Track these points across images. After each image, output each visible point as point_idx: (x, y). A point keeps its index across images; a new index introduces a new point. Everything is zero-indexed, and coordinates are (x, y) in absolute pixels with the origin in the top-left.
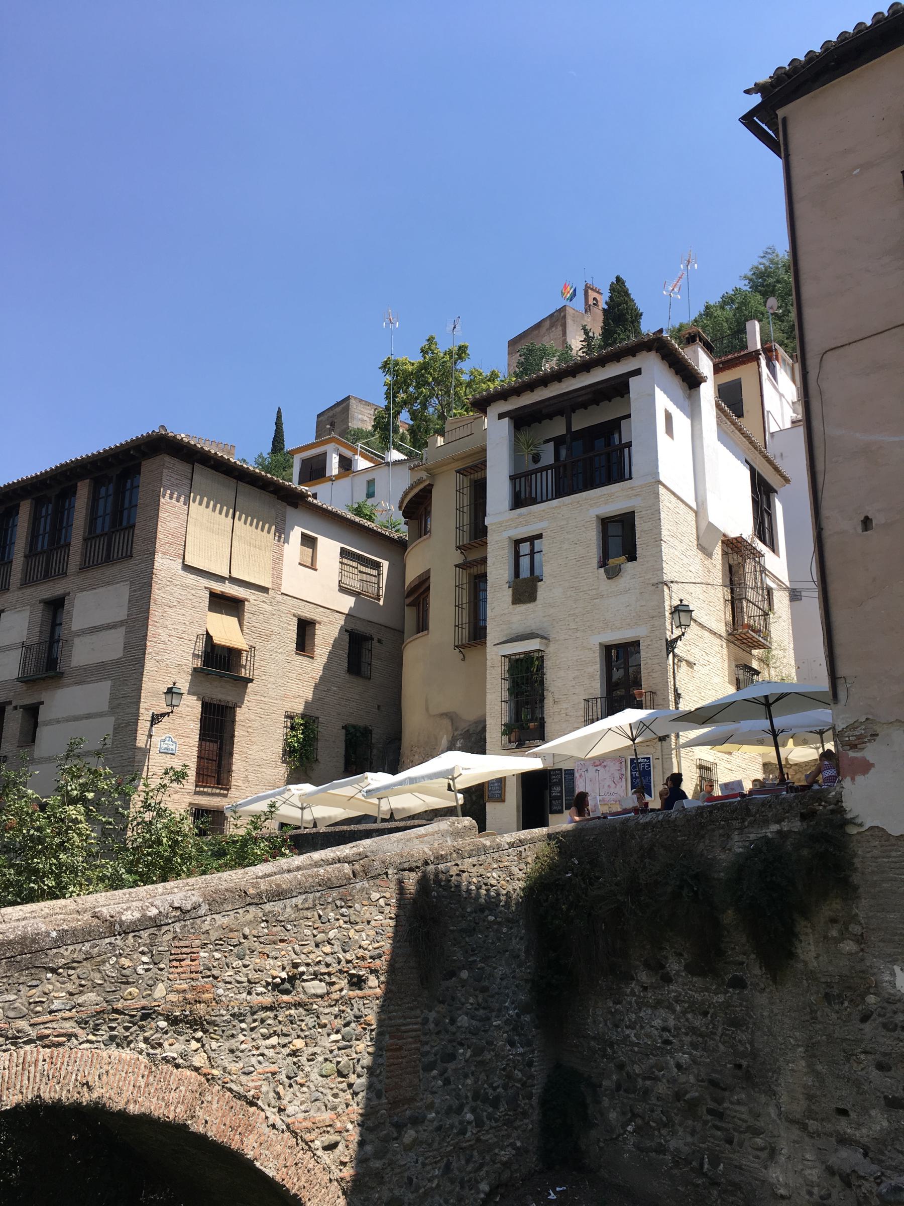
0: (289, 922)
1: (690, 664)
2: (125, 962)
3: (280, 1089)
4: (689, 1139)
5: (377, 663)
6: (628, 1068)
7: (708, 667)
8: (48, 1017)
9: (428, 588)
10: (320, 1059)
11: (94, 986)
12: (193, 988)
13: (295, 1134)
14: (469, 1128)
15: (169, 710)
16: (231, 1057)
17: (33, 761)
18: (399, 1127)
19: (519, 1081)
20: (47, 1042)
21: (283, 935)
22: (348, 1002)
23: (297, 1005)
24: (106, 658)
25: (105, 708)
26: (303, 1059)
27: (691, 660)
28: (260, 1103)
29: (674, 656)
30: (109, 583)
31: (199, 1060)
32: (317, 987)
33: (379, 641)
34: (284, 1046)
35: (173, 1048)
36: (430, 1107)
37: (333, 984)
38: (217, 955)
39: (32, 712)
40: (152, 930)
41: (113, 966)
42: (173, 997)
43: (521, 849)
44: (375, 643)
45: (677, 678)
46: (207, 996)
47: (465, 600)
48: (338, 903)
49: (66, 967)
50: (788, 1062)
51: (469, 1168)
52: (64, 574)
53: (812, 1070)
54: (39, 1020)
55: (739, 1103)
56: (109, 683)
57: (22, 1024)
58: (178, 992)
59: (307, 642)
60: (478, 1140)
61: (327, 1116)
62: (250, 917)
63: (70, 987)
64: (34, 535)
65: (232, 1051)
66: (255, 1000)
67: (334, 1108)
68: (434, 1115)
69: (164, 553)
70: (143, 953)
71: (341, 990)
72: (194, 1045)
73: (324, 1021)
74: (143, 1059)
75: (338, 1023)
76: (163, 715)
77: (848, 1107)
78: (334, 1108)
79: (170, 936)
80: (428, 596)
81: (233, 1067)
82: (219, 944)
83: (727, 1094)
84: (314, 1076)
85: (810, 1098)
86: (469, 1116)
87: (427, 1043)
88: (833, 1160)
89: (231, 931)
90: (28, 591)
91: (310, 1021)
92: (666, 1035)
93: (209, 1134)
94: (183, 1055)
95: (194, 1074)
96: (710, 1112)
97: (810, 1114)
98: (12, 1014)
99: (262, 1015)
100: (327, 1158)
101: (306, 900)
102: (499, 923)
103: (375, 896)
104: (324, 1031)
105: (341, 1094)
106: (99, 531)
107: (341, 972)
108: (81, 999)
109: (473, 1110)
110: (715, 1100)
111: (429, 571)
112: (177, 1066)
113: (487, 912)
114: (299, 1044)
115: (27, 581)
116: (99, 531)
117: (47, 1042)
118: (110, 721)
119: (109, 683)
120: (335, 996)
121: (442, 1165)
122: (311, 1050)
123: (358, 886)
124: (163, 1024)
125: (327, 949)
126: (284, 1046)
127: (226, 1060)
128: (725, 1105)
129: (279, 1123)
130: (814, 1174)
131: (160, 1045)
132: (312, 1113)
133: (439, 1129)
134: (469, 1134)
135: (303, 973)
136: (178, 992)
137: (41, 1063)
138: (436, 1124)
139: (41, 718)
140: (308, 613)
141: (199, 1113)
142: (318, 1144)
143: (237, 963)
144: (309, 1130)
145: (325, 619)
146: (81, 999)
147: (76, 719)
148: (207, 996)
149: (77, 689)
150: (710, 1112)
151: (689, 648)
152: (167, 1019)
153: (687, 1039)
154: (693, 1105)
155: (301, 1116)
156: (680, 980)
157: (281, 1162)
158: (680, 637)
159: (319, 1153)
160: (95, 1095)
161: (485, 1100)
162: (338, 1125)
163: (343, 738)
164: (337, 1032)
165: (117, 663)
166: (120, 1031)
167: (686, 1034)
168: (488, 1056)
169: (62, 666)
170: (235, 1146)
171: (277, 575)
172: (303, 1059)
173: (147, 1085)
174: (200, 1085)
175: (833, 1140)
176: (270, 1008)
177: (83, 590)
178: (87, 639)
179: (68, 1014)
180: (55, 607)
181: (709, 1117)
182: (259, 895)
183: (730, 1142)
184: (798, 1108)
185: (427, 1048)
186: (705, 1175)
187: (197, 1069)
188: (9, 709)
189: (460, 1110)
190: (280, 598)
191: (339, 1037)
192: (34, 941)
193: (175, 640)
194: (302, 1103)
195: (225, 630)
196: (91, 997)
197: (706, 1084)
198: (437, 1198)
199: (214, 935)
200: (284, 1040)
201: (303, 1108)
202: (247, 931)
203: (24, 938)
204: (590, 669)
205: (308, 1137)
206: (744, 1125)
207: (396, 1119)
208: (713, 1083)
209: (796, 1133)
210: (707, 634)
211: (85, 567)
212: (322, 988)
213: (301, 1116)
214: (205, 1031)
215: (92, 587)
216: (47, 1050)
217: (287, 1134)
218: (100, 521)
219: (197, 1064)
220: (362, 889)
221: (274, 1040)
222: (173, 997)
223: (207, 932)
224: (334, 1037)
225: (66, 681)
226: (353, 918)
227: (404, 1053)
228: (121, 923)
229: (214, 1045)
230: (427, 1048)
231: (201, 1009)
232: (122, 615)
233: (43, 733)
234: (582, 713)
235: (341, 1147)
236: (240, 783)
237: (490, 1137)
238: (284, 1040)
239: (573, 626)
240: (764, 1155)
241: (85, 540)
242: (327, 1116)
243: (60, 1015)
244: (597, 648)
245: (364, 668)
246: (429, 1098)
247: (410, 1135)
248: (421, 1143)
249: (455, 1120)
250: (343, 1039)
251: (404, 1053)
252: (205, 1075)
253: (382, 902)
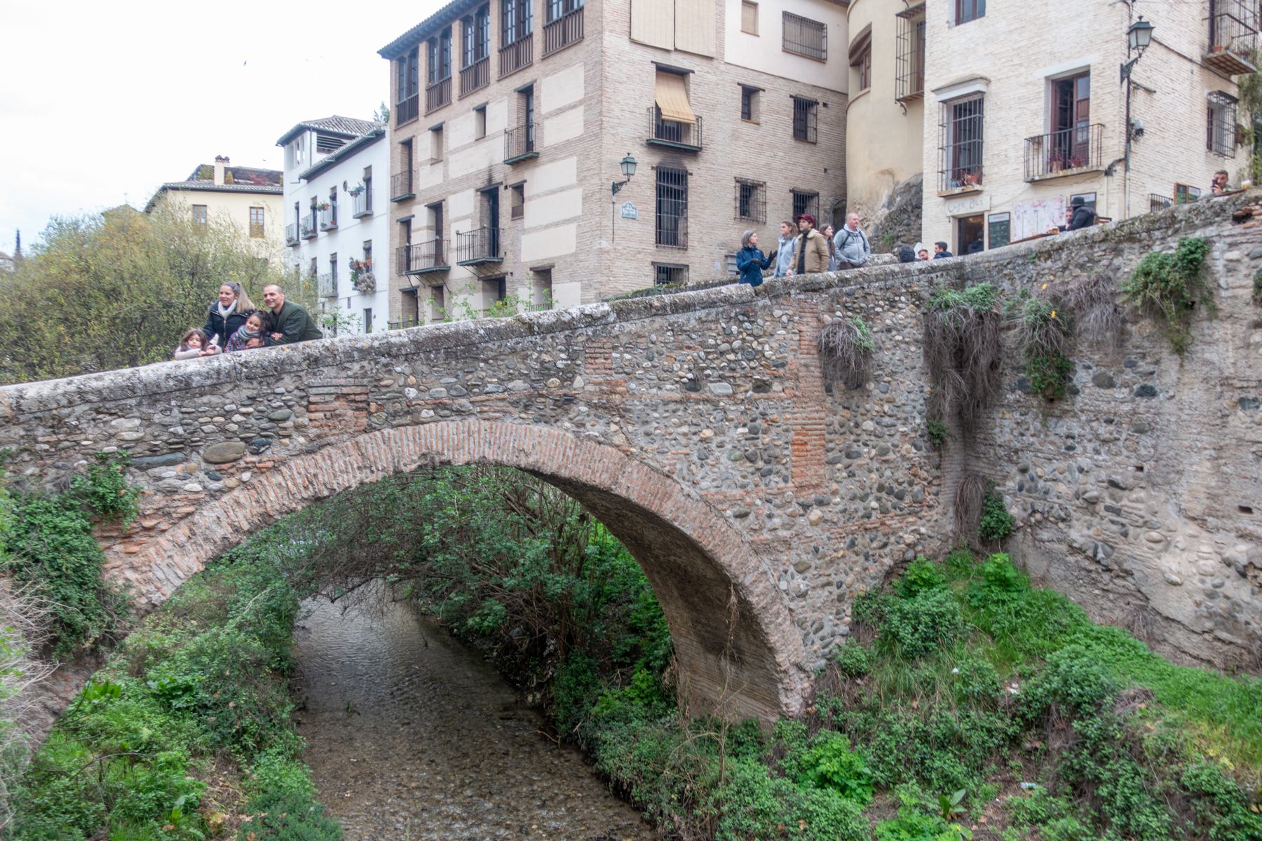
0: (694, 332)
1: (1149, 91)
2: (546, 358)
3: (693, 467)
4: (1085, 532)
5: (821, 122)
6: (1031, 472)
7: (1173, 96)
8: (483, 397)
9: (869, 45)
10: (729, 446)
11: (521, 374)
12: (608, 383)
13: (707, 503)
14: (874, 513)
15: (625, 178)
16: (648, 439)
17: (524, 231)
18: (806, 507)
19: (925, 479)
20: (485, 415)
21: (688, 343)
22: (752, 401)
23: (706, 401)
24: (570, 137)
25: (574, 180)
26: (713, 446)
27: (1152, 87)
28: (675, 477)
29: (1129, 83)
30: (567, 66)
31: (619, 439)
32: (723, 388)
33: (825, 105)
34: (695, 434)
35: (595, 429)
36: (835, 493)
37: (739, 386)
38: (627, 356)
39: (519, 188)
40: (567, 332)
41: (536, 360)
42: (590, 388)
43: (933, 275)
44: (820, 107)
45: (1131, 107)
46: (620, 389)
47: (907, 49)
48: (741, 318)
49: (495, 358)
50: (1191, 465)
51: (874, 545)
52: (531, 65)
53: (1217, 470)
54: (479, 398)
55: (1137, 501)
56: (575, 158)
57: (464, 401)
58: (595, 384)
59: (753, 109)
60: (883, 524)
61: (737, 492)
62: (656, 325)
63: (502, 375)
64: (431, 65)
65: (647, 434)
66: (664, 394)
67: (743, 487)
68: (838, 500)
69: (611, 31)
70: (561, 351)
71: (746, 391)
72: (613, 427)
73: (731, 416)
74: (570, 435)
75: (745, 419)
76: (621, 184)
77: (1253, 505)
78: (743, 487)
79: (584, 338)
80: (869, 55)
81: (649, 447)
82: (629, 348)
83: (1126, 493)
84: (724, 459)
85: (1212, 497)
86: (874, 504)
87: (831, 441)
88: (1229, 553)
89: (639, 336)
90: (505, 82)
91: (720, 415)
92: (1070, 442)
93: (632, 497)
94: (604, 435)
95: (614, 450)
96: (1108, 509)
97: (1212, 512)
98: (453, 393)
99: (672, 406)
100: (737, 524)
101: (708, 314)
102: (907, 343)
103: (777, 313)
104: (732, 424)
105: (750, 476)
106: (555, 17)
107: (746, 376)
108: (510, 385)
109: (878, 499)
110: (1112, 497)
111: (870, 26)
112: (600, 443)
113: (894, 333)
114: (708, 433)
115: (504, 75)
116: (555, 17)
117: (485, 415)
118: (578, 193)
119: (575, 158)
120: (740, 396)
121: (848, 541)
122: (719, 439)
123: (760, 304)
124: (584, 409)
125: (731, 357)
126: (695, 434)
127: (642, 440)
128: (1123, 503)
129: (693, 494)
130: (1211, 564)
131: (584, 425)
132: (723, 489)
133: (844, 511)
134: (873, 518)
135: (709, 376)
136: (595, 384)
137: (483, 432)
138: (841, 507)
139: (526, 195)
140: (751, 82)
141: (622, 480)
142: (729, 513)
143: (647, 364)
144: (721, 502)
145: (769, 86)
146: (510, 385)
147: (553, 192)
148: (620, 389)
149: (549, 166)
150: (1108, 509)
151: (1149, 74)
152: (589, 404)
153: (1090, 446)
154: (1092, 502)
155: (713, 490)
156: (1087, 391)
157: (697, 523)
158: (1136, 60)
159: (732, 520)
160: (531, 460)
161: (890, 492)
162: (748, 500)
163: (791, 201)
164: (745, 425)
165: (580, 139)
166: (548, 412)
167: (1090, 441)
168: (891, 456)
169: (537, 149)
170: (654, 509)
171: (721, 45)
172: (713, 446)
173: (574, 455)
174: (621, 459)
175: (1233, 534)
176: (681, 402)
177: (547, 75)
178: (554, 120)
179: (501, 396)
180: (527, 93)
181: (1106, 514)
182: (664, 307)
183: (1125, 535)
184: (1197, 509)
185: (831, 445)
186: (1098, 562)
187: (617, 446)
188: (501, 188)
189: (864, 498)
190: (723, 67)
191: (746, 430)
192: (465, 336)
193: (627, 115)
194: (714, 480)
195: (676, 104)
196: (518, 384)
197: (1105, 485)
198: (842, 565)
199: (624, 339)
200: (694, 429)
201: (715, 484)
202: (654, 337)
203: (457, 333)
204: (1034, 106)
205: (719, 507)
206: (1141, 521)
207: (802, 500)
208: (1113, 484)
209: (1192, 528)
210: (1174, 58)
211: (545, 58)
212: (726, 388)
213: (713, 490)
214: (622, 417)
215: (554, 71)
216: (487, 423)
217: (701, 504)
218: (555, 7)
219: (617, 443)
220: (764, 307)
221: (685, 429)
222: (590, 388)
223: (617, 336)
224: (741, 430)
225: (541, 160)
226: (755, 332)
227: (809, 447)
228: (540, 326)
229: (631, 428)
230: (831, 445)
231: (616, 399)
232: (579, 94)
233: (528, 207)
234: (1022, 153)
235: (751, 517)
236: (696, 244)
237: (894, 523)
238: (694, 429)
239: (1017, 61)
240: (1158, 547)
241: (500, 51)
242: (737, 492)
243: (495, 396)
244: (1043, 81)
245: (811, 135)
246: (835, 486)
247: (815, 513)
248: (826, 521)
249: (859, 505)
250: (750, 432)
251: (809, 447)
252: (624, 451)
253: (784, 319)
